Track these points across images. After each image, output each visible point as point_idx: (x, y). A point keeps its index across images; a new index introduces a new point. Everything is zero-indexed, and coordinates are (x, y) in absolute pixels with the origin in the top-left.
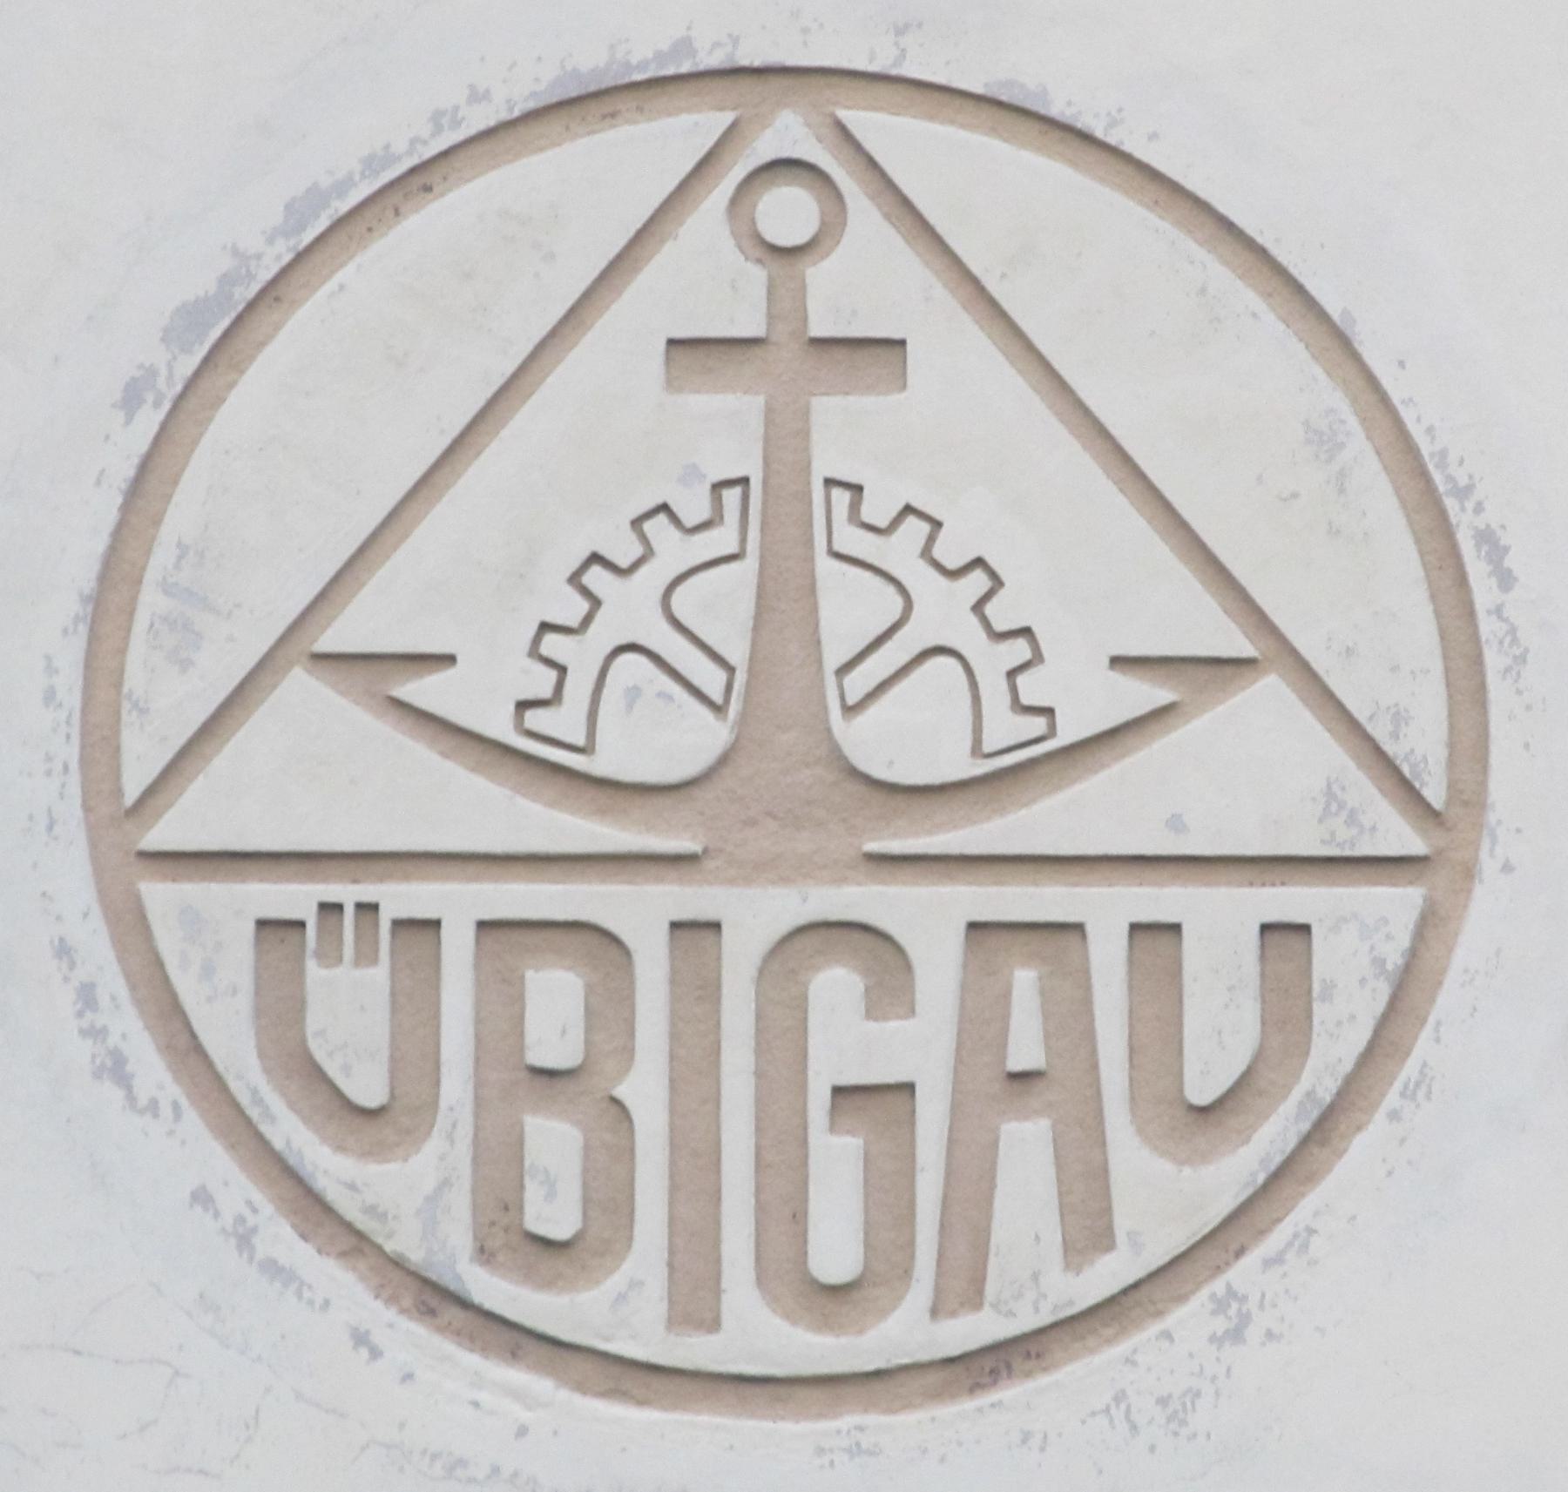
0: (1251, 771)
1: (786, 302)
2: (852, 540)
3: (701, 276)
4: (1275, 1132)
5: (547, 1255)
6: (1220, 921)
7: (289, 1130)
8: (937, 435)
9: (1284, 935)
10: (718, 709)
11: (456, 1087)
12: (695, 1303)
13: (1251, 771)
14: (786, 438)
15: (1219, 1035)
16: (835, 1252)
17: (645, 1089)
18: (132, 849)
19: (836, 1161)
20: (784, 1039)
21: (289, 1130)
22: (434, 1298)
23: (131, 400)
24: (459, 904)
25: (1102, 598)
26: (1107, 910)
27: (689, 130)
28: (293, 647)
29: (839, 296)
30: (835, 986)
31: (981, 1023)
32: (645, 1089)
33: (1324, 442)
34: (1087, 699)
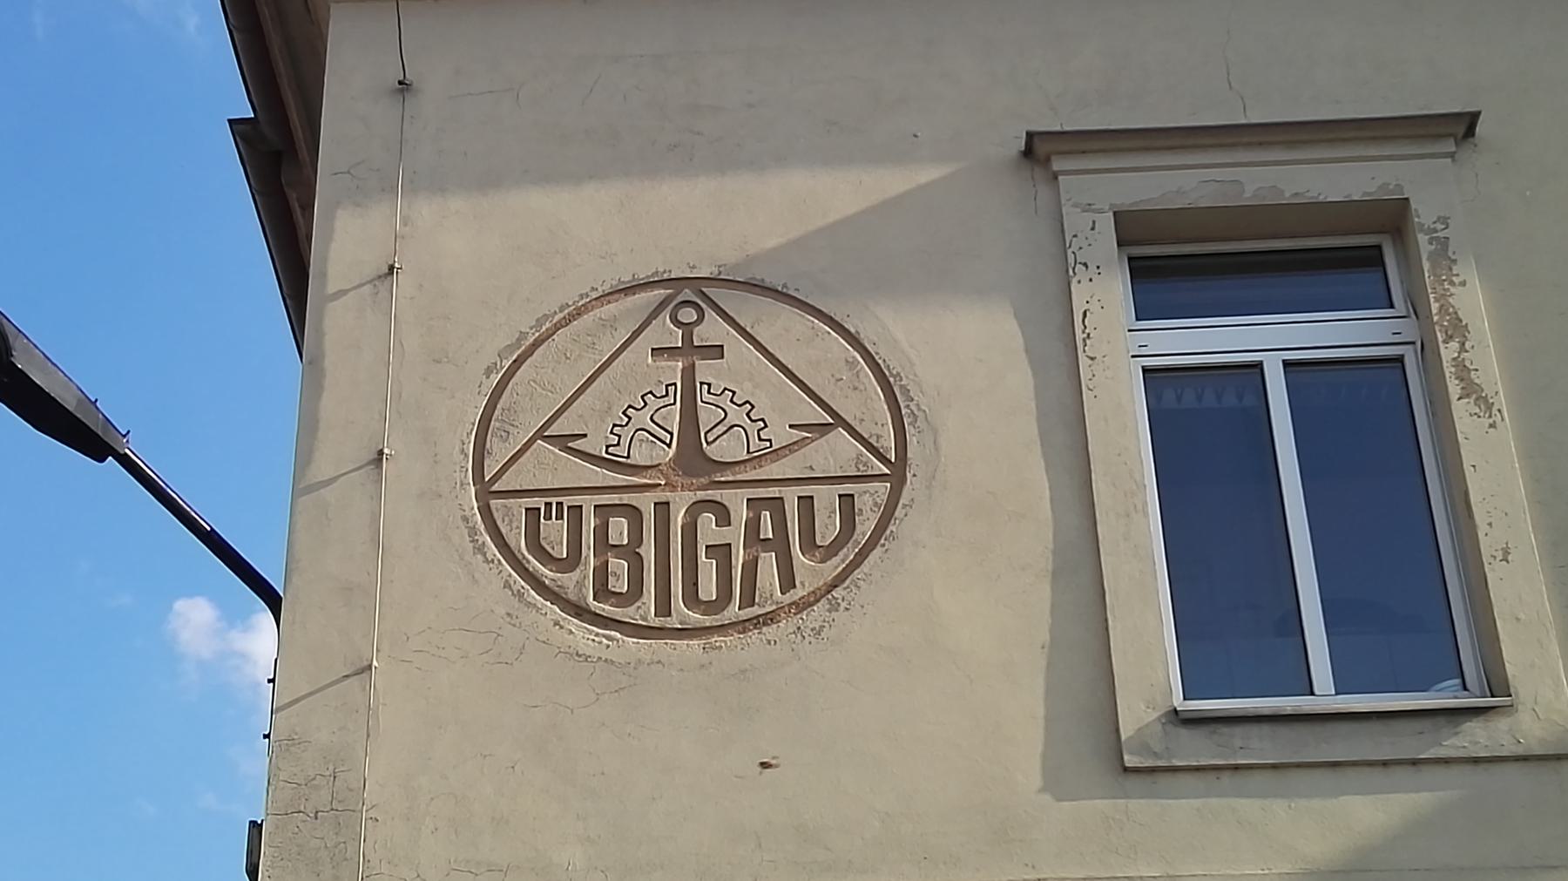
0: (838, 452)
1: (687, 338)
2: (711, 398)
3: (666, 332)
4: (848, 553)
5: (623, 600)
6: (826, 498)
7: (534, 564)
8: (736, 371)
9: (847, 499)
10: (669, 446)
11: (588, 551)
12: (664, 608)
13: (838, 452)
14: (689, 373)
15: (828, 527)
16: (709, 588)
17: (649, 551)
18: (486, 493)
19: (708, 570)
20: (690, 530)
21: (534, 564)
22: (580, 611)
23: (488, 372)
24: (588, 502)
25: (783, 409)
26: (791, 495)
27: (660, 293)
28: (540, 434)
29: (702, 335)
30: (708, 520)
31: (753, 526)
32: (649, 551)
33: (852, 364)
34: (781, 435)
